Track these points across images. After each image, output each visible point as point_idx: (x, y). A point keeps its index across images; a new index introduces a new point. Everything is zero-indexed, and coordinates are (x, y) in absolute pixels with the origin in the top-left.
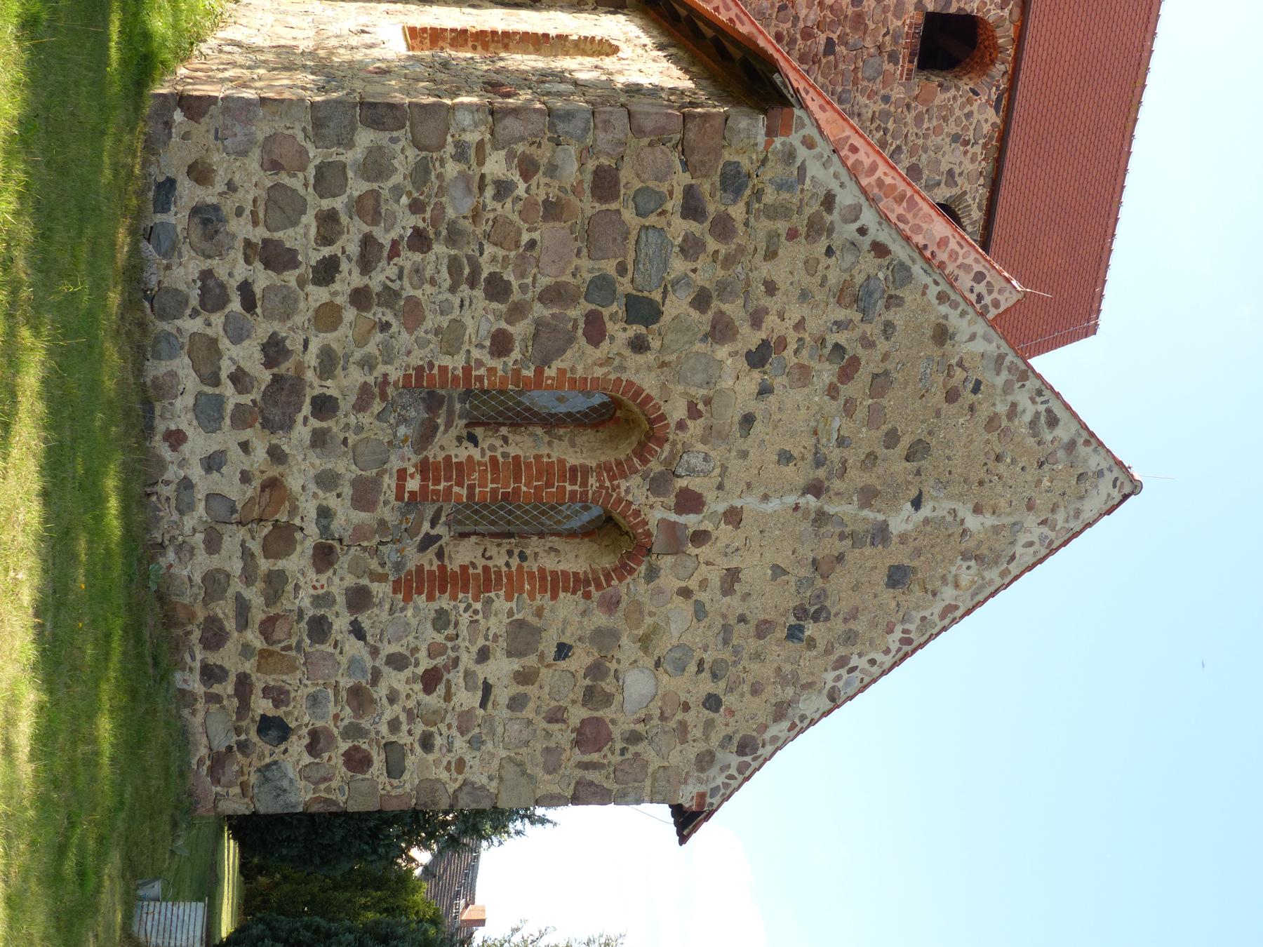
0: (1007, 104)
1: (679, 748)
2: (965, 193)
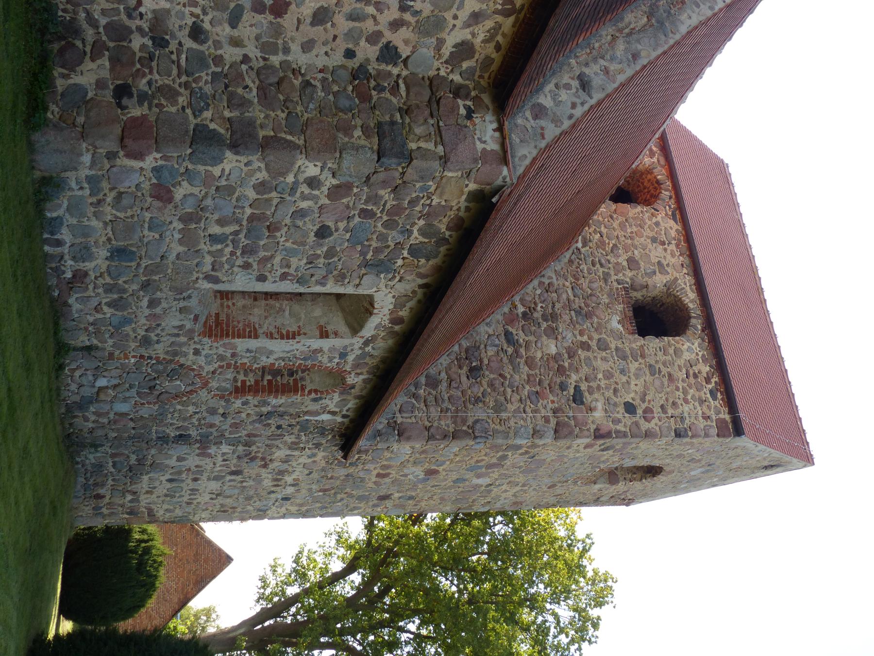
0: (680, 213)
1: (336, 448)
2: (676, 279)
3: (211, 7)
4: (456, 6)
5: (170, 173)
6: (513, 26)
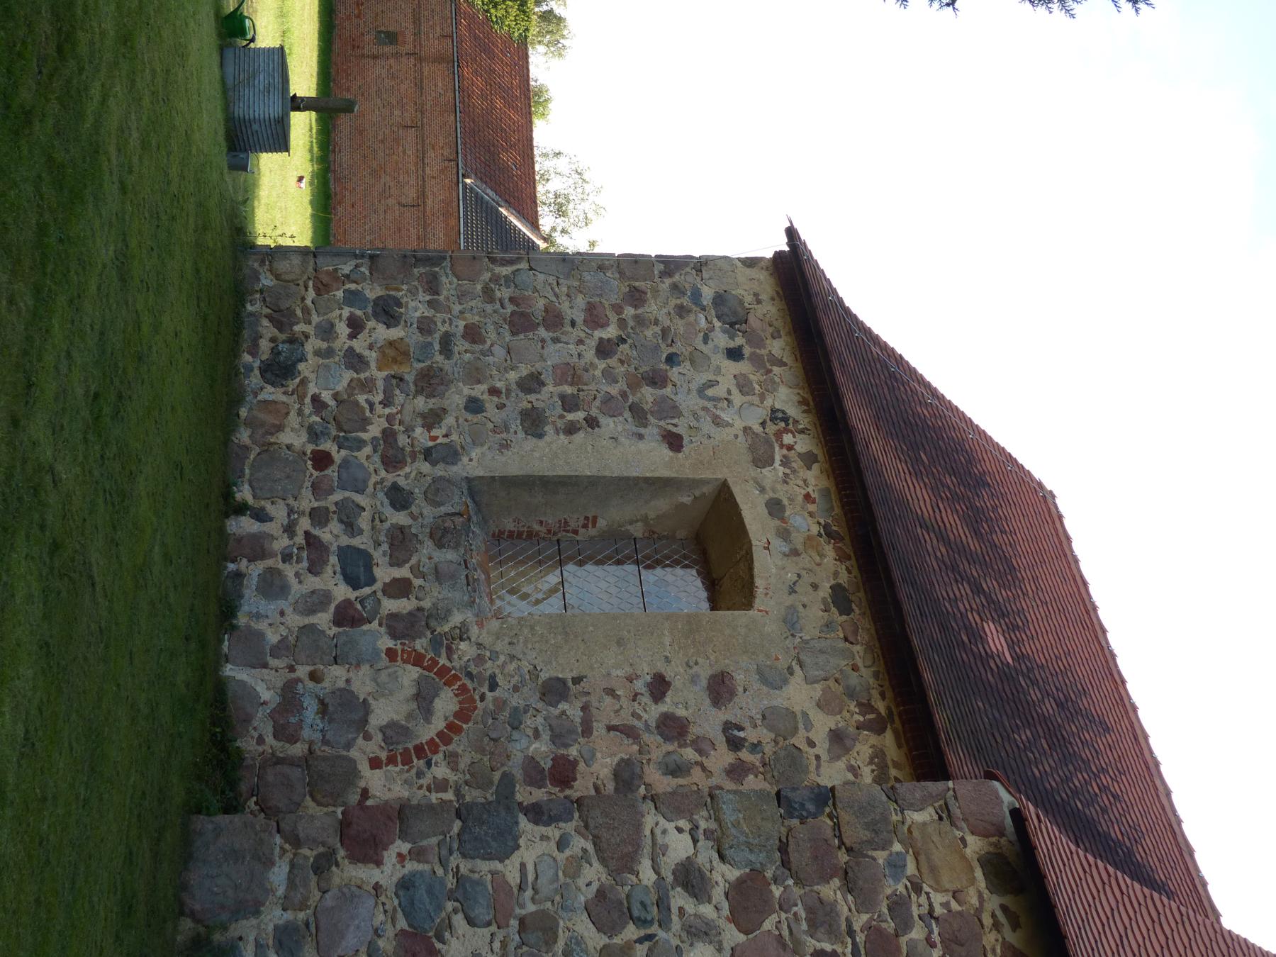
3: (466, 783)
4: (801, 726)
5: (430, 892)
6: (899, 746)
